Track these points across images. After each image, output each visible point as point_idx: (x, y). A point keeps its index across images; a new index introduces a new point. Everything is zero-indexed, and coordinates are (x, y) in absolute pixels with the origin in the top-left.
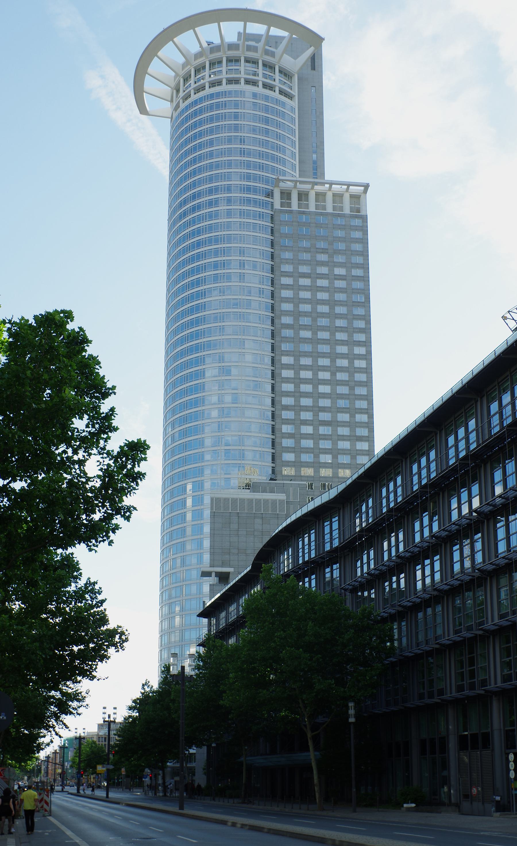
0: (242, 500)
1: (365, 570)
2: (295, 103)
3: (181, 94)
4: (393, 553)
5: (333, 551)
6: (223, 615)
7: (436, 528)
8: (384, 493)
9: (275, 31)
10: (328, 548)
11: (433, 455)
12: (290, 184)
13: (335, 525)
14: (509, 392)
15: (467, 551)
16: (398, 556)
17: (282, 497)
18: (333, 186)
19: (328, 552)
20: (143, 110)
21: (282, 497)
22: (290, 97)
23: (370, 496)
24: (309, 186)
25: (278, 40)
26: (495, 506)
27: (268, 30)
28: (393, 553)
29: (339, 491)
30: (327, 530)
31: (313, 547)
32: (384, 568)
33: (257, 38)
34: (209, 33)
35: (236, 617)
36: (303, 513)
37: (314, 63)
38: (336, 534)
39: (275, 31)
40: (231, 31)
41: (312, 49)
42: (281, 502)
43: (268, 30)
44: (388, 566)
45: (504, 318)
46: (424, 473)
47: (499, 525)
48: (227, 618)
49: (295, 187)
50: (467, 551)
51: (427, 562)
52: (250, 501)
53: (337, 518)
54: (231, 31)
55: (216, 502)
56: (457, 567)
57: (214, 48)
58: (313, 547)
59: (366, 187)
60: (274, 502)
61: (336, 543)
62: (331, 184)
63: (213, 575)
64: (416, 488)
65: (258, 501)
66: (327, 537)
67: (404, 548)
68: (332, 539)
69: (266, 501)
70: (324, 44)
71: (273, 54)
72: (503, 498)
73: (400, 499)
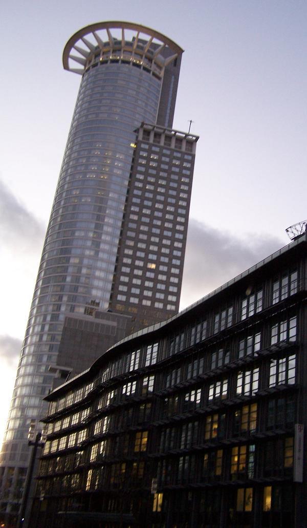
0: (87, 322)
1: (195, 375)
2: (161, 83)
3: (92, 63)
4: (173, 383)
5: (151, 367)
6: (63, 401)
7: (227, 361)
8: (193, 332)
9: (155, 41)
10: (147, 364)
11: (231, 310)
12: (150, 128)
13: (155, 349)
14: (287, 278)
15: (248, 379)
16: (175, 386)
17: (115, 324)
18: (177, 134)
19: (147, 367)
20: (66, 66)
21: (115, 324)
22: (159, 78)
23: (182, 332)
24: (162, 131)
25: (155, 46)
26: (271, 351)
27: (152, 40)
28: (173, 383)
29: (162, 326)
30: (149, 351)
31: (132, 362)
32: (166, 392)
33: (145, 42)
34: (116, 33)
35: (81, 399)
36: (125, 341)
37: (177, 63)
38: (155, 355)
39: (155, 41)
40: (130, 35)
41: (176, 55)
42: (113, 327)
43: (152, 40)
44: (168, 391)
45: (287, 231)
46: (223, 322)
47: (272, 365)
48: (57, 408)
49: (153, 129)
50: (248, 379)
51: (219, 384)
52: (92, 323)
53: (157, 344)
54: (130, 35)
55: (68, 320)
56: (239, 390)
57: (118, 43)
58: (132, 362)
59: (197, 138)
60: (109, 327)
61: (154, 362)
62: (176, 132)
63: (58, 371)
64: (216, 332)
65: (98, 325)
66: (148, 357)
67: (203, 372)
68: (134, 365)
69: (103, 325)
70: (183, 54)
71: (152, 53)
72: (243, 361)
73: (203, 338)
